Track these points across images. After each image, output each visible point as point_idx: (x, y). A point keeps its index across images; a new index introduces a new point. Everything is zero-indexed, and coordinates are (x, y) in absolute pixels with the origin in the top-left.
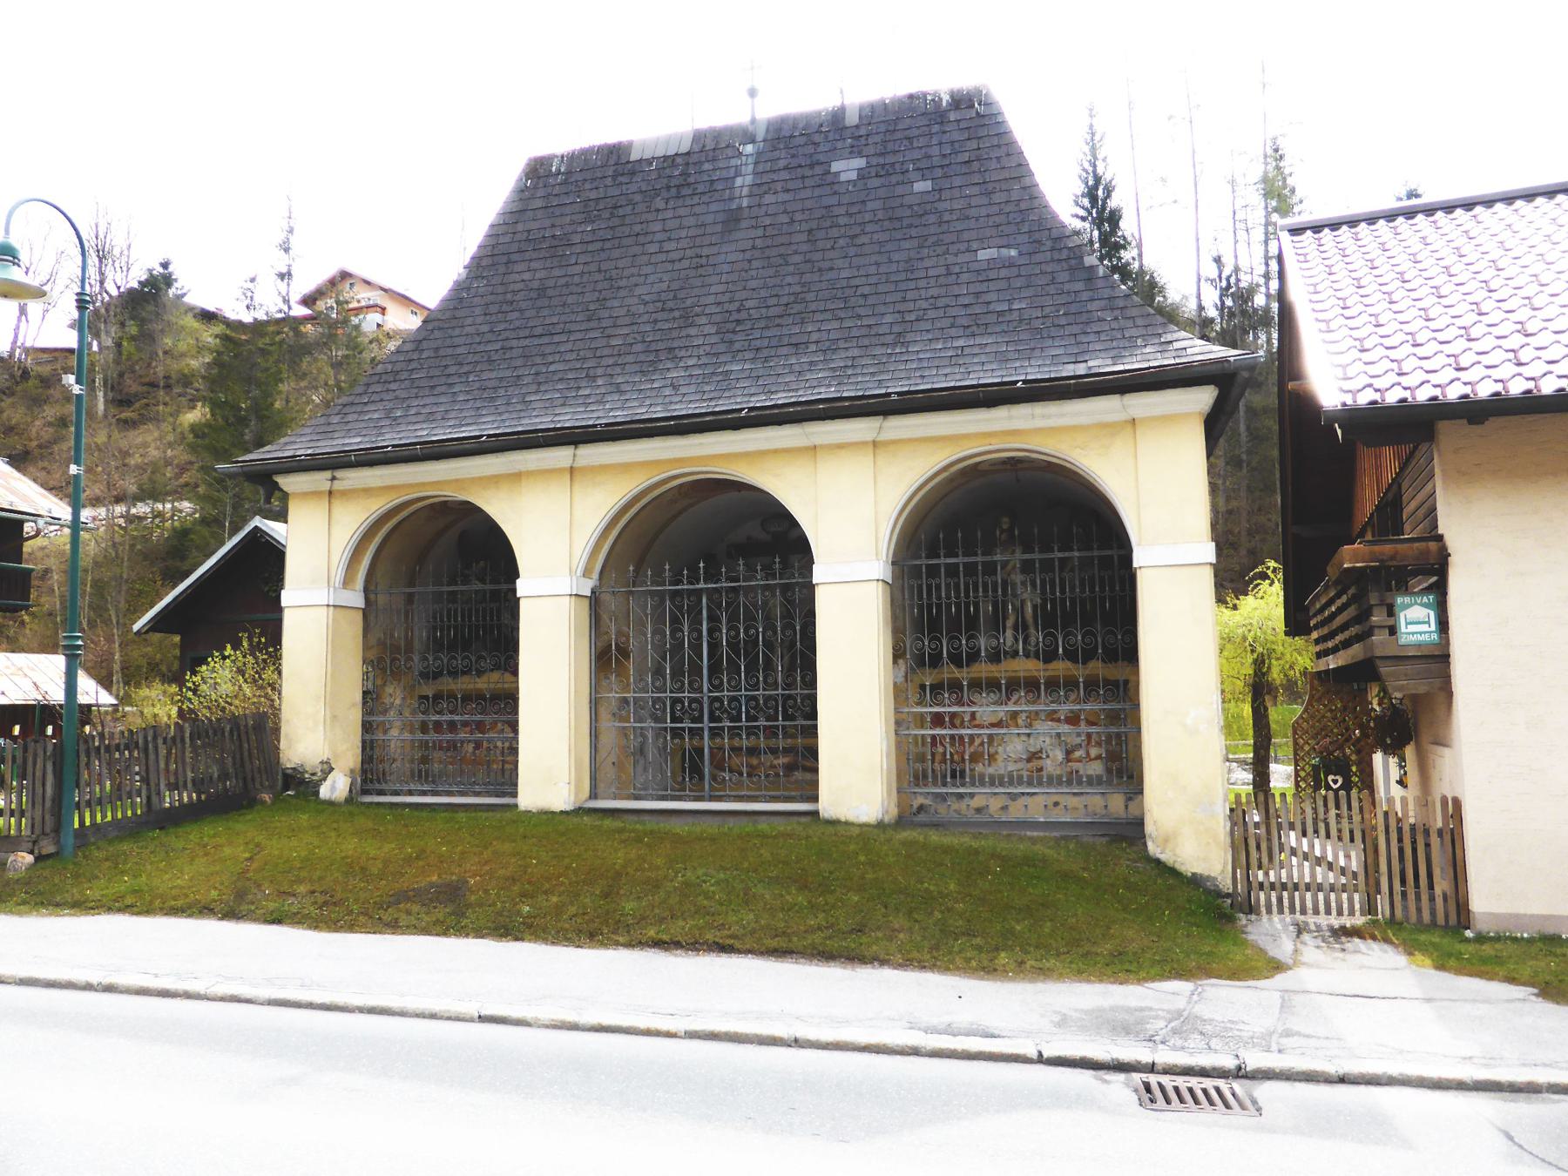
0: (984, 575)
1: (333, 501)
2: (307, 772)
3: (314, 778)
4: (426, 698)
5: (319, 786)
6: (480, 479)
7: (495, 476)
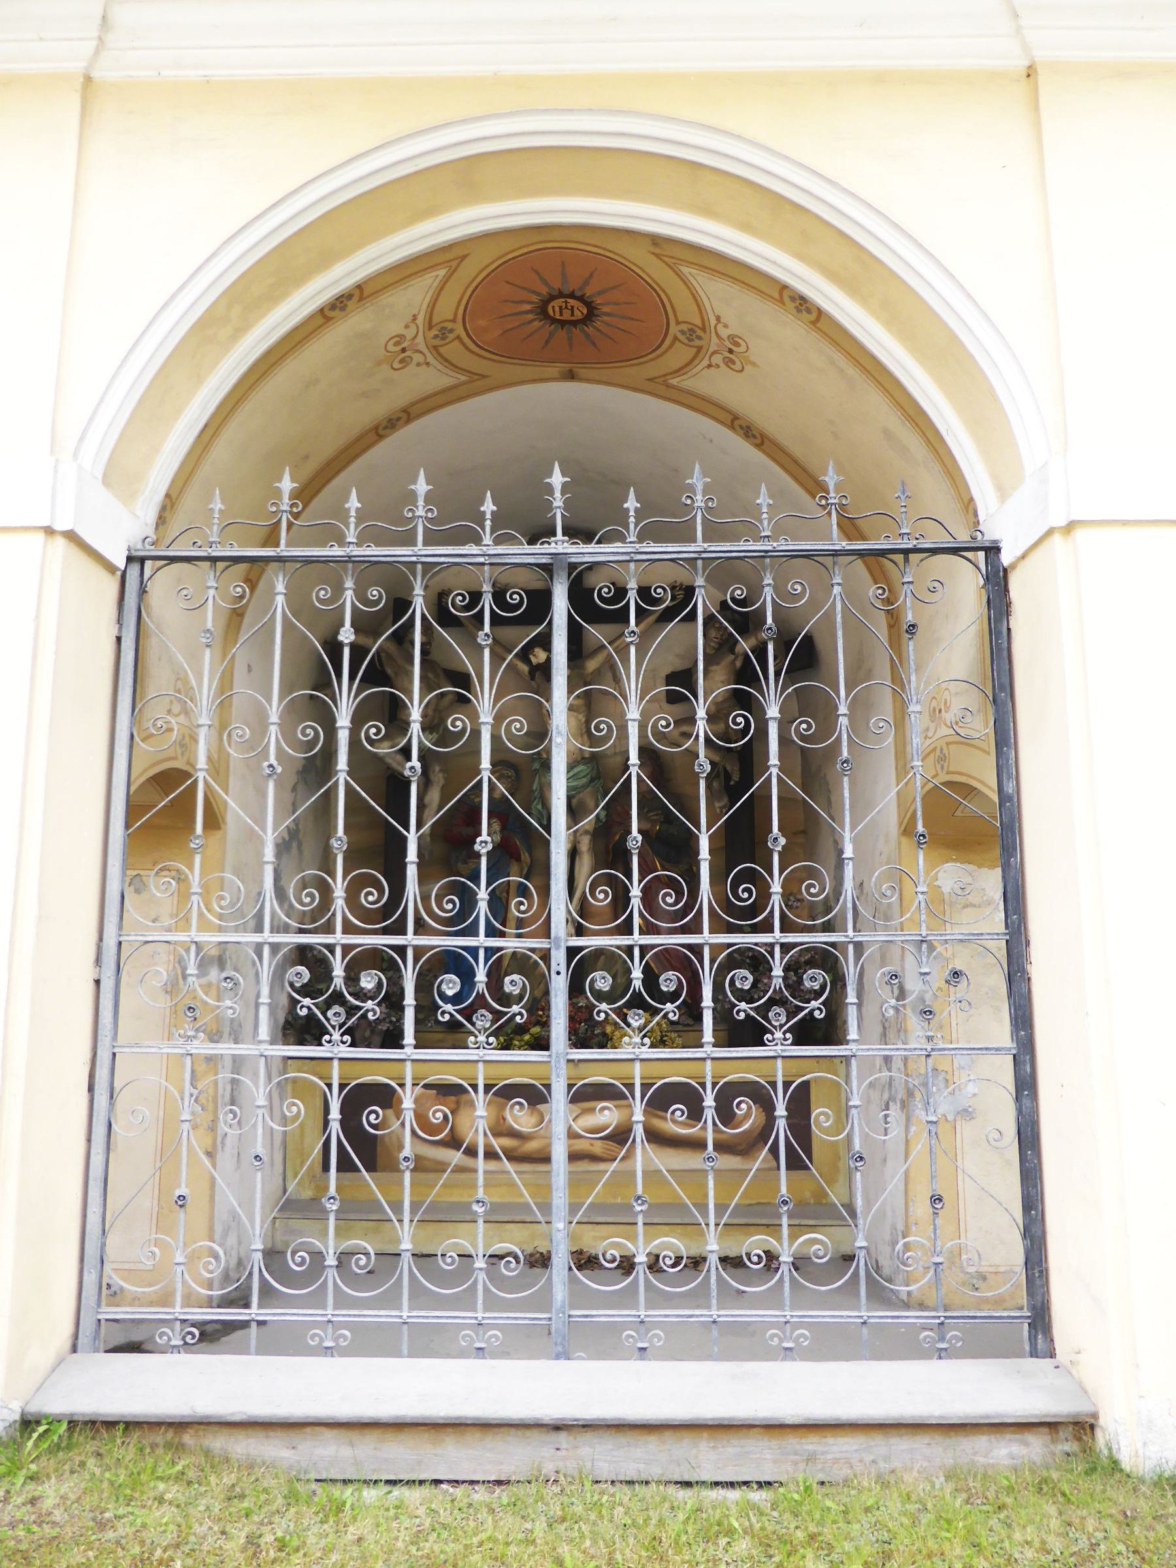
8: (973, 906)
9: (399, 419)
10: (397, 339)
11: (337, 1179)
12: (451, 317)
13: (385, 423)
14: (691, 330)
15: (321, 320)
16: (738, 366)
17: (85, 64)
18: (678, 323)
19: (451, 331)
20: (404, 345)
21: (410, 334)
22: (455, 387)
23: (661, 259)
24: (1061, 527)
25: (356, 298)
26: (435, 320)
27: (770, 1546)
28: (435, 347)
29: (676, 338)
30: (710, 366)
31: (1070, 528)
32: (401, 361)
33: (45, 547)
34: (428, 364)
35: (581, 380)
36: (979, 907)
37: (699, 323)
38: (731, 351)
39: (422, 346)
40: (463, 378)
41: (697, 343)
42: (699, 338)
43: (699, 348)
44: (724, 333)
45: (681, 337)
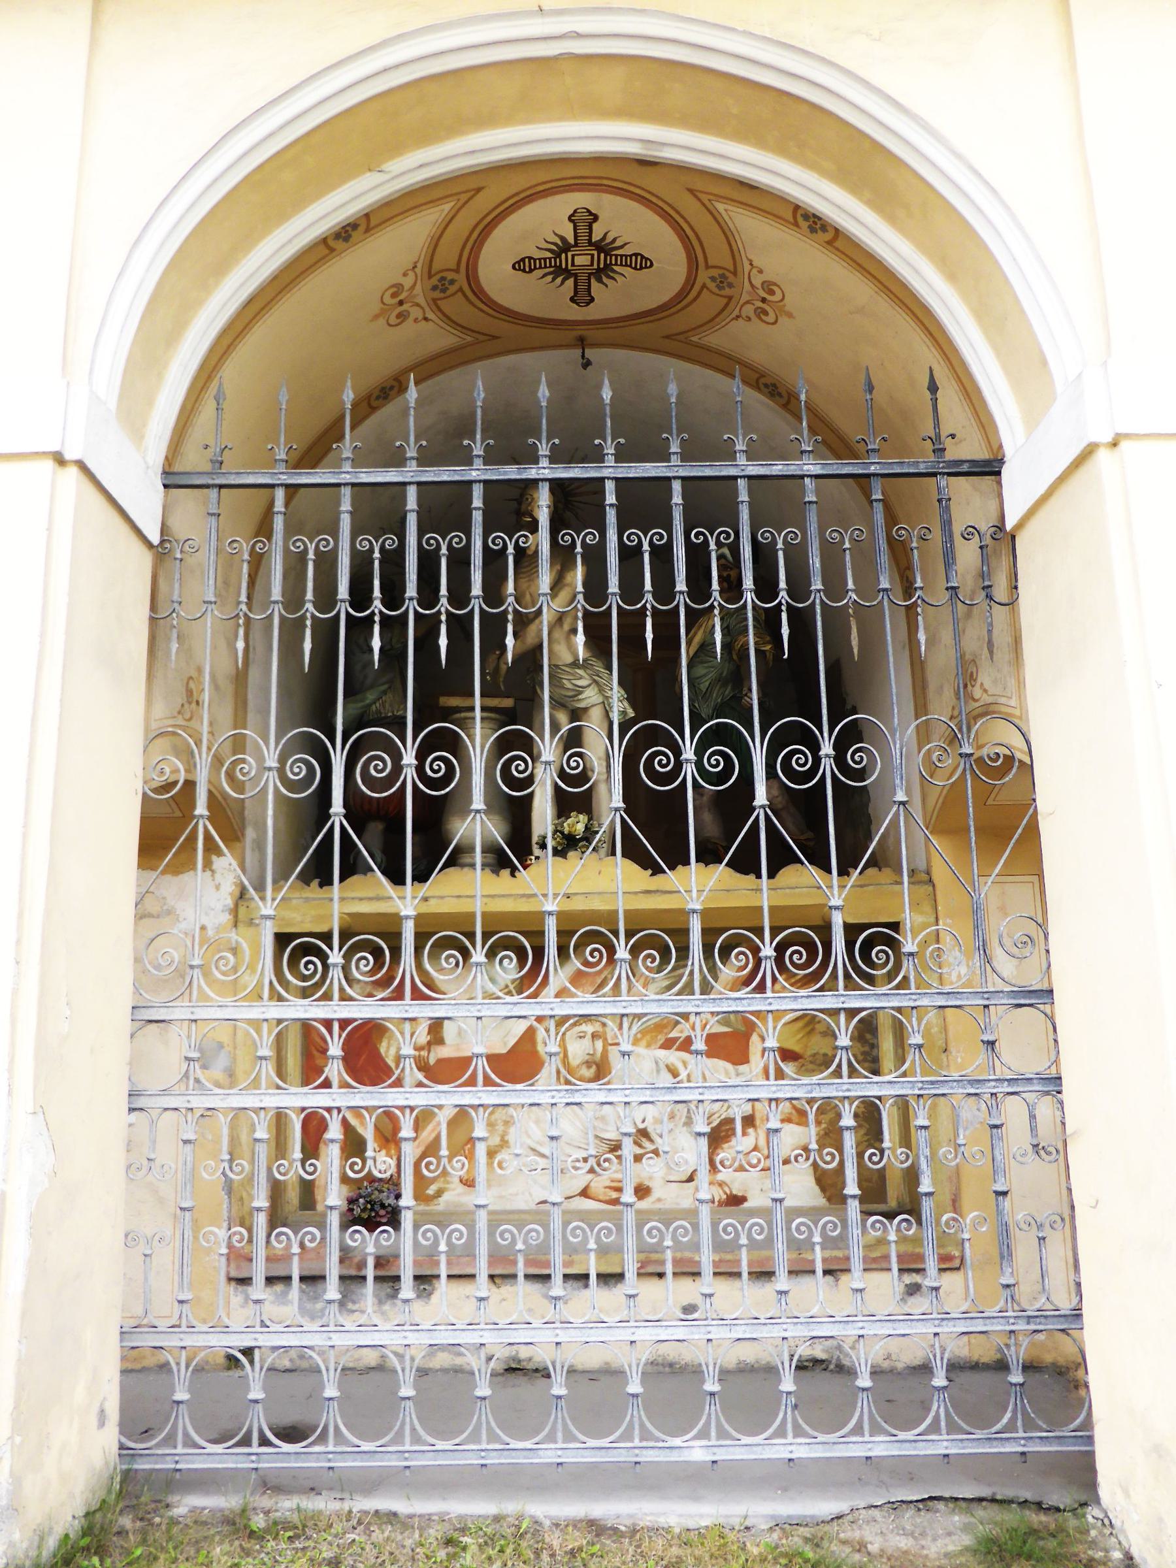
8: (150, 916)
9: (392, 388)
10: (394, 290)
11: (291, 1269)
12: (454, 266)
13: (376, 393)
14: (723, 276)
15: (323, 250)
16: (771, 318)
18: (707, 267)
20: (401, 297)
21: (408, 282)
23: (696, 197)
25: (362, 229)
26: (436, 267)
28: (435, 300)
29: (704, 286)
34: (426, 319)
36: (158, 917)
39: (421, 300)
44: (758, 281)
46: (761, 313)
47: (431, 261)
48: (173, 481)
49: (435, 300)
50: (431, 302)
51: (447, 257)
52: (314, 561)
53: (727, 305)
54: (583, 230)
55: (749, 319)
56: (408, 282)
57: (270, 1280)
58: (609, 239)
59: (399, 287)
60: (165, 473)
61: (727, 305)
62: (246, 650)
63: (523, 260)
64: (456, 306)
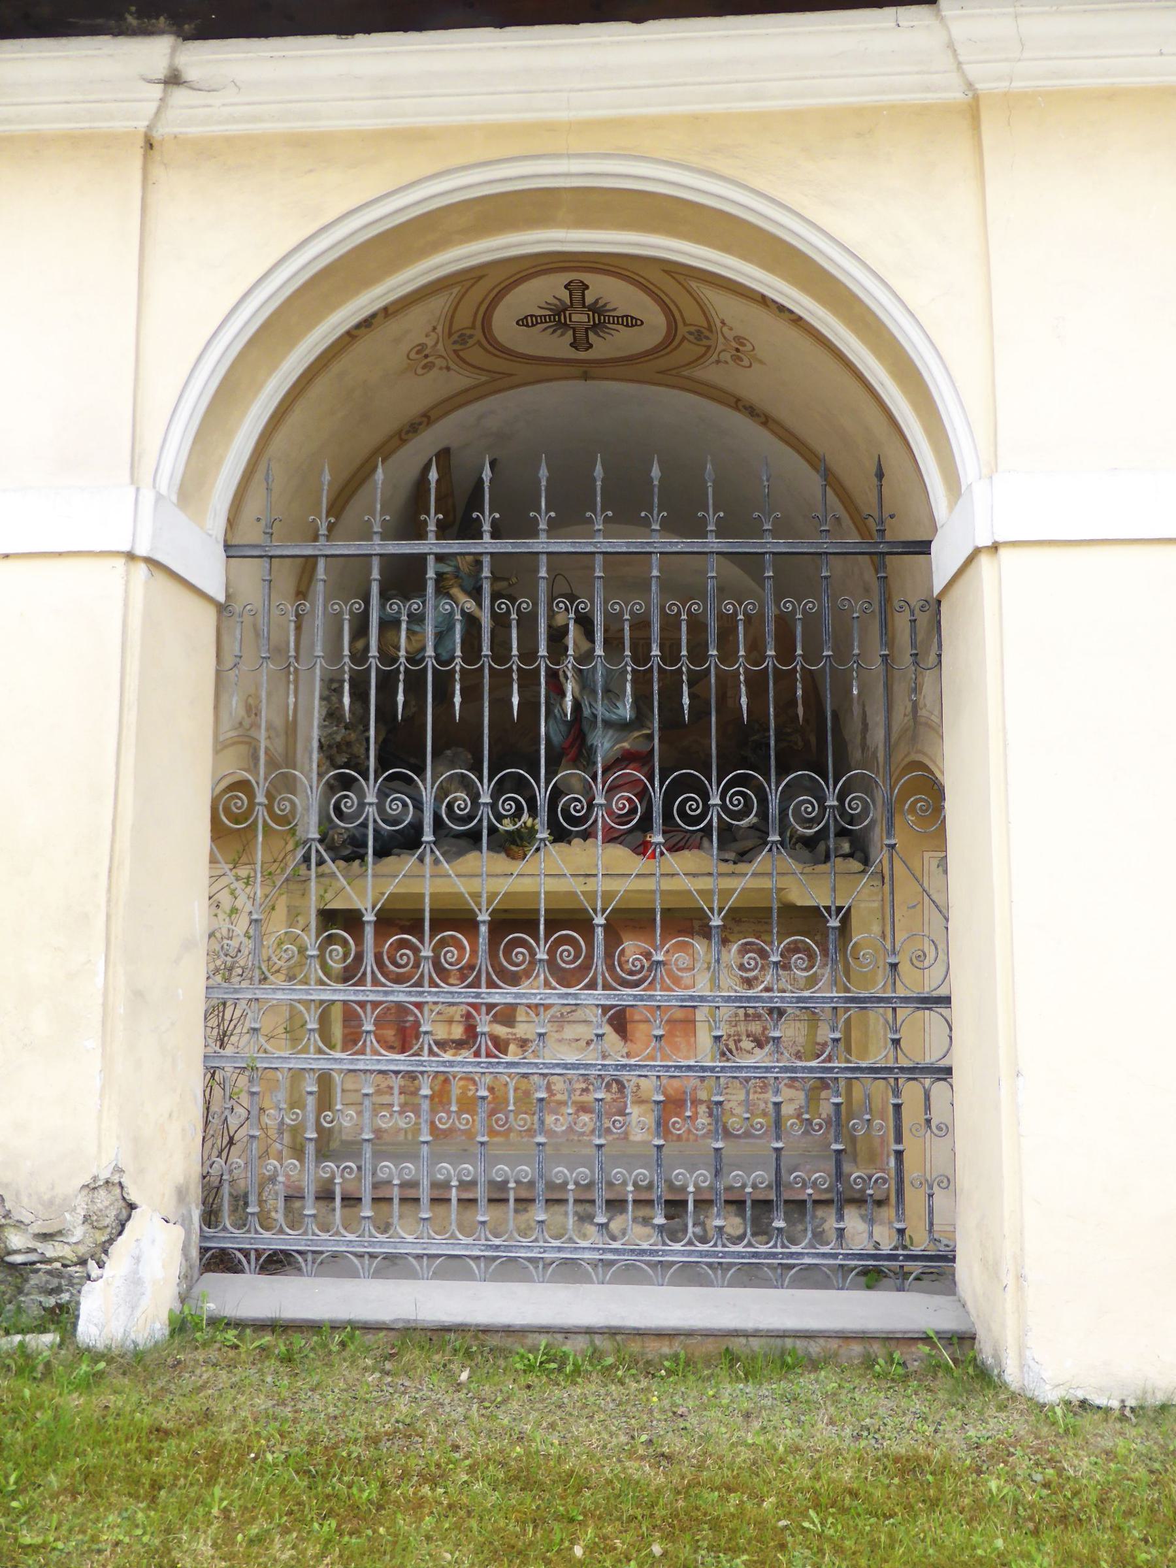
0: (384, 596)
1: (157, 172)
2: (19, 1225)
3: (50, 1250)
4: (350, 920)
5: (75, 1285)
6: (796, 117)
7: (858, 112)
9: (420, 424)
12: (470, 325)
15: (348, 339)
16: (746, 362)
17: (146, 123)
19: (471, 336)
21: (430, 342)
22: (475, 387)
24: (987, 547)
26: (455, 328)
27: (758, 1475)
28: (455, 351)
30: (718, 362)
31: (995, 547)
32: (424, 367)
33: (128, 573)
34: (448, 368)
35: (593, 378)
37: (705, 325)
38: (737, 350)
40: (484, 379)
41: (705, 342)
42: (707, 338)
43: (709, 347)
45: (688, 336)
46: (737, 359)
47: (452, 317)
48: (231, 550)
49: (455, 351)
50: (453, 356)
51: (463, 319)
52: (350, 621)
53: (704, 354)
54: (577, 295)
55: (726, 362)
56: (430, 342)
57: (434, 1201)
58: (601, 303)
59: (423, 346)
60: (227, 547)
61: (704, 354)
62: (296, 704)
63: (526, 318)
64: (475, 355)
